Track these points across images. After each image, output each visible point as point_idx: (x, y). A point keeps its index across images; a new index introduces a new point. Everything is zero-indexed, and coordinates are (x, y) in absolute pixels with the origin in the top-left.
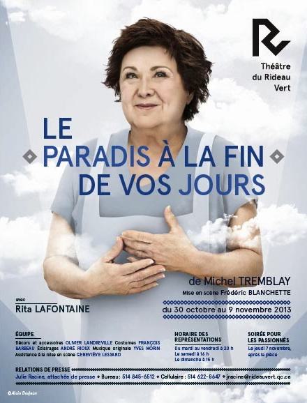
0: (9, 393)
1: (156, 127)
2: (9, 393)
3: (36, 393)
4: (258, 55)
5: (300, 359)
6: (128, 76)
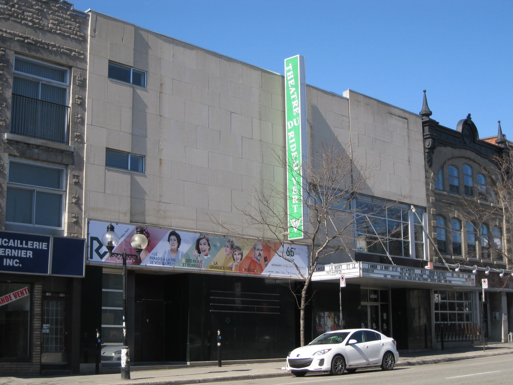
0: (211, 297)
1: (174, 249)
2: (211, 297)
3: (279, 301)
4: (92, 259)
5: (58, 19)
6: (171, 240)
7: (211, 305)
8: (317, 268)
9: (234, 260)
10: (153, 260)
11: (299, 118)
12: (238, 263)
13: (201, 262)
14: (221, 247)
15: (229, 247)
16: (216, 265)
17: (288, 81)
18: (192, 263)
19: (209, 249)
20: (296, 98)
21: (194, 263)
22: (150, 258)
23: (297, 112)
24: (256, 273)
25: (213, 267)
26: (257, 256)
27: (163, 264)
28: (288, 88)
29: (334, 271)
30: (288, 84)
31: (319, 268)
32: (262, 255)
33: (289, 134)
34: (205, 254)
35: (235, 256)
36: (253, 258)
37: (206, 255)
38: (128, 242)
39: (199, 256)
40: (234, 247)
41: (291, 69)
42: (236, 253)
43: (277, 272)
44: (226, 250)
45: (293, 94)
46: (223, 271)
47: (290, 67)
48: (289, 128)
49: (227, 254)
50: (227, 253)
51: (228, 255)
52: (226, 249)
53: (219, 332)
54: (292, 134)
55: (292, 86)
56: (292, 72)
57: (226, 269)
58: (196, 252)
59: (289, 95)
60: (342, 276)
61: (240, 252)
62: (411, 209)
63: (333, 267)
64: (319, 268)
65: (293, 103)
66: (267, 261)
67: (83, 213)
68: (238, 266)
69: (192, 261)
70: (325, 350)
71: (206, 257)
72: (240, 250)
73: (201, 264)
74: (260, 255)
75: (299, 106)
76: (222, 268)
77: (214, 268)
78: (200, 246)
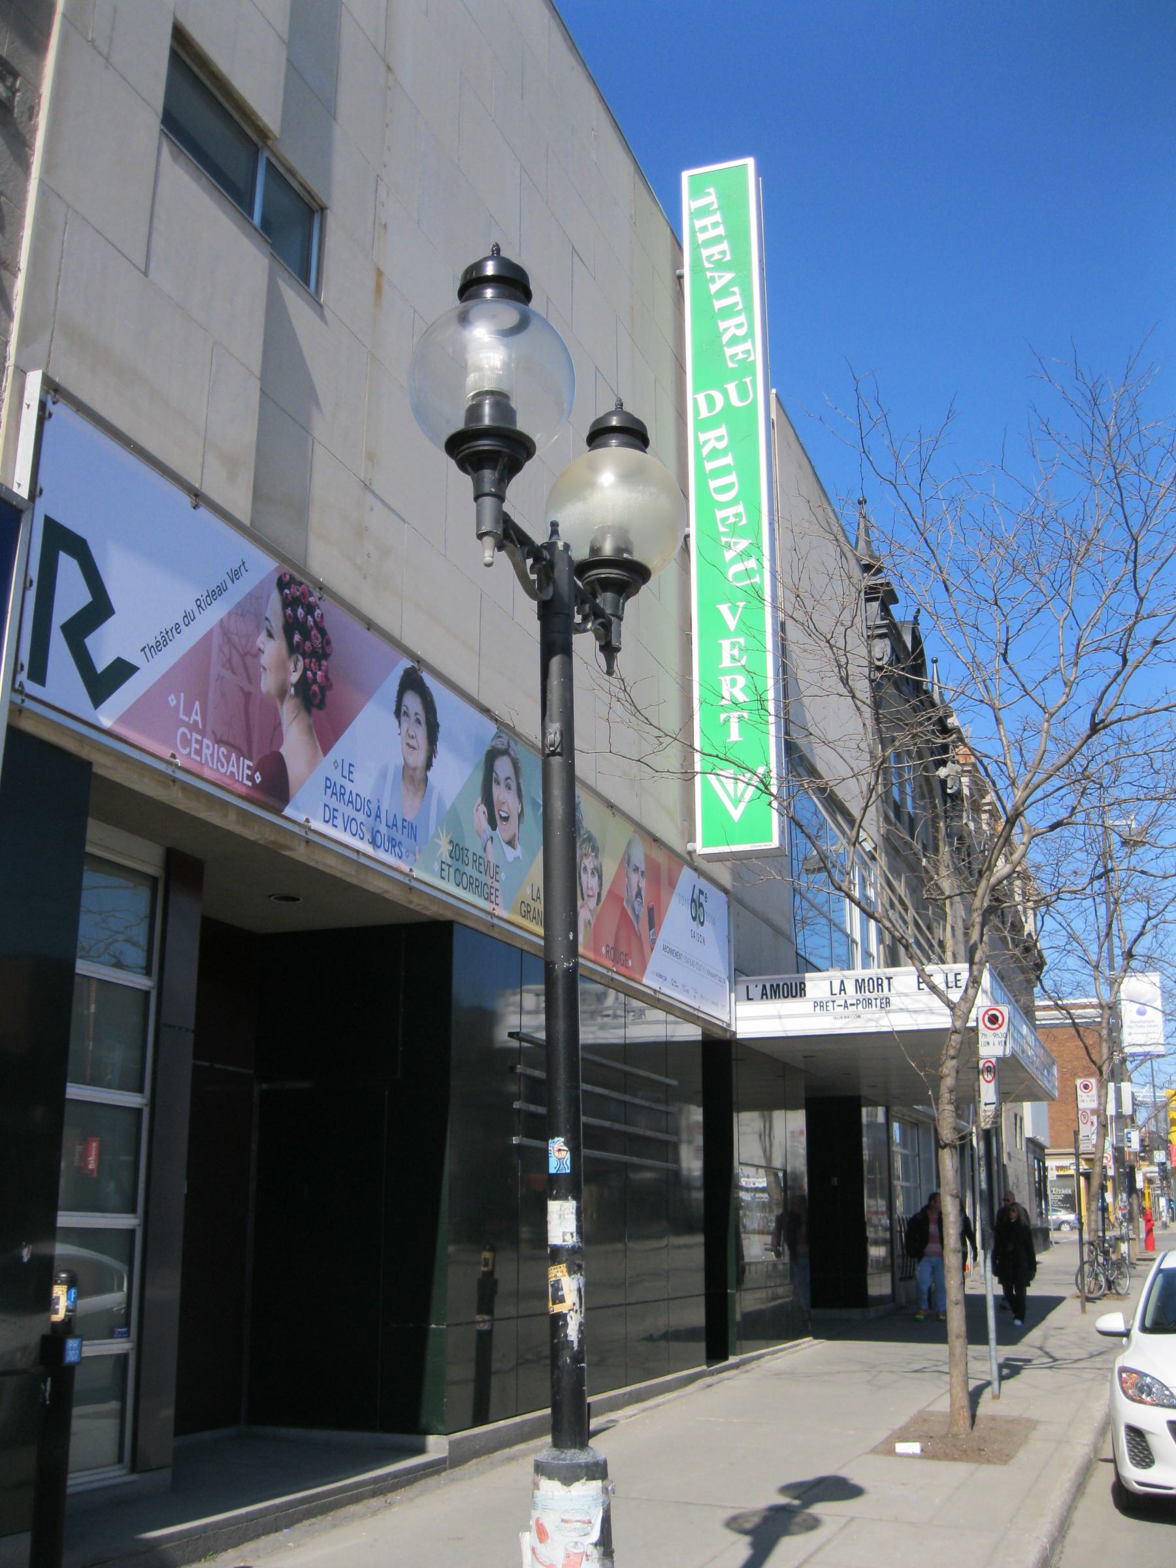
8: (764, 987)
10: (337, 805)
11: (754, 382)
20: (740, 307)
22: (327, 787)
26: (634, 897)
27: (373, 842)
29: (851, 997)
31: (778, 985)
32: (643, 893)
33: (703, 437)
36: (625, 904)
38: (236, 649)
43: (674, 984)
45: (724, 292)
47: (711, 198)
48: (704, 413)
54: (719, 439)
55: (720, 266)
56: (717, 217)
60: (991, 1012)
62: (860, 840)
63: (845, 981)
64: (778, 985)
65: (722, 325)
67: (15, 327)
70: (1147, 1375)
71: (509, 851)
75: (750, 334)
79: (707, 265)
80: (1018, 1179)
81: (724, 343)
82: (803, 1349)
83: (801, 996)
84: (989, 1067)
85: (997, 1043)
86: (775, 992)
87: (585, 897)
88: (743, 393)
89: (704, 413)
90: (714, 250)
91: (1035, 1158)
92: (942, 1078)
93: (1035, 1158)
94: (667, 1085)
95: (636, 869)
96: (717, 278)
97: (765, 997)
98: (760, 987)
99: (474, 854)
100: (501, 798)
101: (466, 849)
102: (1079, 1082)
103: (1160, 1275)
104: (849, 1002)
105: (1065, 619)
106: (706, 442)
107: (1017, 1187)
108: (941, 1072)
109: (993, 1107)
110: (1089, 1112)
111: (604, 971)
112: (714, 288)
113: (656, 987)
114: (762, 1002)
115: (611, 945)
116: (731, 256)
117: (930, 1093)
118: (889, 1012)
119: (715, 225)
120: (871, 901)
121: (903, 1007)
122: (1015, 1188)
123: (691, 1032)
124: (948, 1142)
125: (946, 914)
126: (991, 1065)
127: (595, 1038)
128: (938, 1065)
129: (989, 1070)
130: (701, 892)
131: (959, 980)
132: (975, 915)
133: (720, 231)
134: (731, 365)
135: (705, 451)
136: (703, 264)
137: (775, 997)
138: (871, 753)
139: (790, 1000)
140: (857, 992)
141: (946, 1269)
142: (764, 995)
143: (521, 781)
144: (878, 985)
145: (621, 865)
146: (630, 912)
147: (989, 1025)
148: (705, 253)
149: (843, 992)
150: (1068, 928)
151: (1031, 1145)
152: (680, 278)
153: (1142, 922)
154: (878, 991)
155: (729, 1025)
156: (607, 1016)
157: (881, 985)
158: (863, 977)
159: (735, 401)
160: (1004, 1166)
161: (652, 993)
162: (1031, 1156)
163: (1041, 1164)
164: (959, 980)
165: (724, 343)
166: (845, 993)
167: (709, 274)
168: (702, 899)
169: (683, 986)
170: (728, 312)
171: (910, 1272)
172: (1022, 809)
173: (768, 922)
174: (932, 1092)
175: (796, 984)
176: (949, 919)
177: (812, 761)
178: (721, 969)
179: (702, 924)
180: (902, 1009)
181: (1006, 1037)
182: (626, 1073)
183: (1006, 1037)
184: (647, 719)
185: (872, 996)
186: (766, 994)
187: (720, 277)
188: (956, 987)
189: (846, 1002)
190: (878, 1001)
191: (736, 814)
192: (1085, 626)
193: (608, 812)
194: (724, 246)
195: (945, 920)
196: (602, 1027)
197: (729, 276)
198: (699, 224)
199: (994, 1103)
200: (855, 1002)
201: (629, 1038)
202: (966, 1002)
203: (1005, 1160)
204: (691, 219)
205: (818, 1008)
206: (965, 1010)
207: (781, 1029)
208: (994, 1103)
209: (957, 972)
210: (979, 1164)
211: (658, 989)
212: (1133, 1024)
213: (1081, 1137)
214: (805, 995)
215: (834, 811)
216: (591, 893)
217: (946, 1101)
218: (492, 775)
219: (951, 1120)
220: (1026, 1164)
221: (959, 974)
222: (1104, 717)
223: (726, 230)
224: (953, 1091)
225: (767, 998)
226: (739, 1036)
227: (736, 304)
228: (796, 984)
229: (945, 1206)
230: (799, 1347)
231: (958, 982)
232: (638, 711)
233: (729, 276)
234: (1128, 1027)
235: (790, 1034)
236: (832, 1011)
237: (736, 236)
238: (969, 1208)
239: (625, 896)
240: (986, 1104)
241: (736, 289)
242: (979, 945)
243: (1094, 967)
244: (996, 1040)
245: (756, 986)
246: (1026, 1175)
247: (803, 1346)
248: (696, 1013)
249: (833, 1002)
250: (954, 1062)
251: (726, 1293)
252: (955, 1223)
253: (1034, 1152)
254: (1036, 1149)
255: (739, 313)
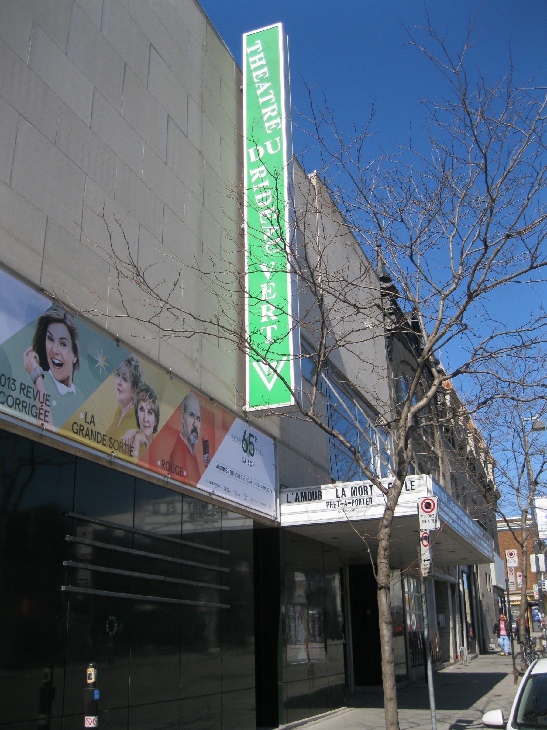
7: (67, 567)
8: (297, 494)
9: (139, 426)
12: (147, 436)
13: (47, 400)
14: (109, 370)
15: (129, 380)
16: (91, 427)
17: (251, 71)
18: (16, 394)
19: (74, 366)
20: (274, 100)
21: (22, 397)
23: (276, 128)
24: (187, 481)
25: (82, 430)
28: (251, 83)
30: (250, 78)
31: (305, 493)
32: (198, 430)
33: (252, 172)
34: (60, 378)
35: (141, 414)
36: (181, 435)
37: (64, 382)
39: (40, 379)
40: (140, 385)
41: (261, 49)
42: (144, 404)
43: (226, 490)
44: (121, 388)
45: (265, 93)
46: (109, 450)
47: (259, 46)
49: (121, 401)
50: (123, 396)
51: (123, 403)
52: (120, 385)
53: (92, 671)
55: (262, 80)
56: (262, 55)
57: (116, 447)
58: (32, 359)
59: (254, 98)
61: (153, 406)
63: (345, 489)
64: (305, 493)
65: (264, 111)
66: (209, 453)
68: (148, 446)
69: (18, 384)
71: (62, 389)
72: (154, 402)
73: (45, 408)
74: (194, 430)
75: (279, 114)
76: (107, 442)
77: (84, 432)
78: (49, 345)
79: (256, 80)
80: (489, 607)
81: (265, 120)
82: (337, 715)
83: (319, 499)
84: (426, 536)
85: (430, 521)
86: (304, 497)
87: (142, 426)
88: (275, 146)
89: (253, 159)
90: (260, 72)
91: (499, 596)
92: (379, 541)
93: (499, 596)
94: (221, 554)
95: (192, 415)
96: (261, 86)
97: (297, 500)
98: (295, 494)
99: (22, 384)
100: (55, 350)
101: (13, 379)
102: (507, 552)
103: (530, 680)
104: (347, 502)
105: (453, 237)
106: (254, 175)
107: (488, 612)
108: (379, 537)
109: (428, 562)
110: (513, 568)
111: (162, 478)
112: (259, 92)
113: (211, 491)
114: (296, 503)
115: (167, 459)
116: (269, 74)
117: (369, 551)
118: (371, 507)
119: (260, 59)
120: (388, 456)
121: (380, 503)
122: (487, 612)
123: (249, 523)
124: (383, 585)
125: (439, 467)
126: (427, 535)
127: (203, 529)
128: (377, 531)
129: (425, 538)
130: (251, 435)
131: (414, 485)
132: (401, 430)
133: (263, 62)
134: (268, 132)
135: (253, 180)
136: (253, 80)
137: (304, 501)
138: (389, 377)
139: (313, 501)
140: (352, 496)
141: (383, 675)
142: (297, 500)
143: (77, 343)
144: (365, 490)
145: (178, 409)
146: (185, 441)
147: (425, 509)
148: (255, 74)
149: (344, 496)
150: (502, 471)
151: (496, 590)
152: (242, 90)
153: (541, 465)
154: (365, 494)
155: (276, 518)
156: (209, 515)
157: (367, 490)
158: (355, 486)
159: (270, 151)
160: (480, 601)
161: (207, 495)
162: (496, 595)
163: (502, 599)
164: (414, 485)
165: (265, 120)
166: (345, 496)
167: (256, 85)
168: (252, 440)
169: (235, 492)
170: (267, 104)
171: (418, 662)
172: (427, 356)
173: (310, 460)
174: (370, 551)
175: (316, 492)
176: (441, 469)
177: (344, 374)
178: (269, 483)
179: (252, 455)
180: (379, 504)
181: (436, 517)
182: (182, 545)
183: (436, 517)
184: (158, 295)
185: (361, 497)
186: (298, 499)
187: (263, 86)
188: (412, 489)
189: (346, 501)
190: (365, 500)
191: (269, 386)
192: (466, 239)
193: (168, 376)
194: (265, 70)
195: (439, 471)
196: (206, 522)
197: (267, 85)
198: (251, 60)
199: (429, 560)
200: (351, 501)
201: (223, 527)
202: (395, 489)
203: (481, 598)
204: (247, 58)
205: (329, 506)
206: (395, 494)
207: (308, 519)
208: (429, 560)
209: (412, 480)
210: (422, 600)
211: (211, 492)
212: (543, 523)
213: (509, 583)
214: (321, 499)
215: (352, 397)
216: (147, 425)
217: (382, 557)
218: (46, 334)
219: (385, 570)
220: (493, 599)
221: (414, 481)
222: (476, 288)
223: (266, 61)
224: (386, 550)
225: (299, 501)
226: (282, 525)
227: (271, 99)
228: (316, 492)
229: (382, 630)
230: (335, 714)
231: (413, 487)
232: (152, 290)
233: (267, 85)
234: (541, 525)
235: (313, 522)
236: (337, 507)
237: (272, 64)
238: (459, 624)
239: (181, 430)
240: (425, 561)
241: (271, 91)
242: (405, 452)
243: (516, 490)
244: (430, 519)
245: (293, 494)
246: (493, 605)
247: (338, 713)
248: (247, 509)
249: (338, 502)
250: (387, 530)
251: (277, 685)
252: (389, 642)
253: (498, 593)
254: (499, 592)
255: (273, 104)
